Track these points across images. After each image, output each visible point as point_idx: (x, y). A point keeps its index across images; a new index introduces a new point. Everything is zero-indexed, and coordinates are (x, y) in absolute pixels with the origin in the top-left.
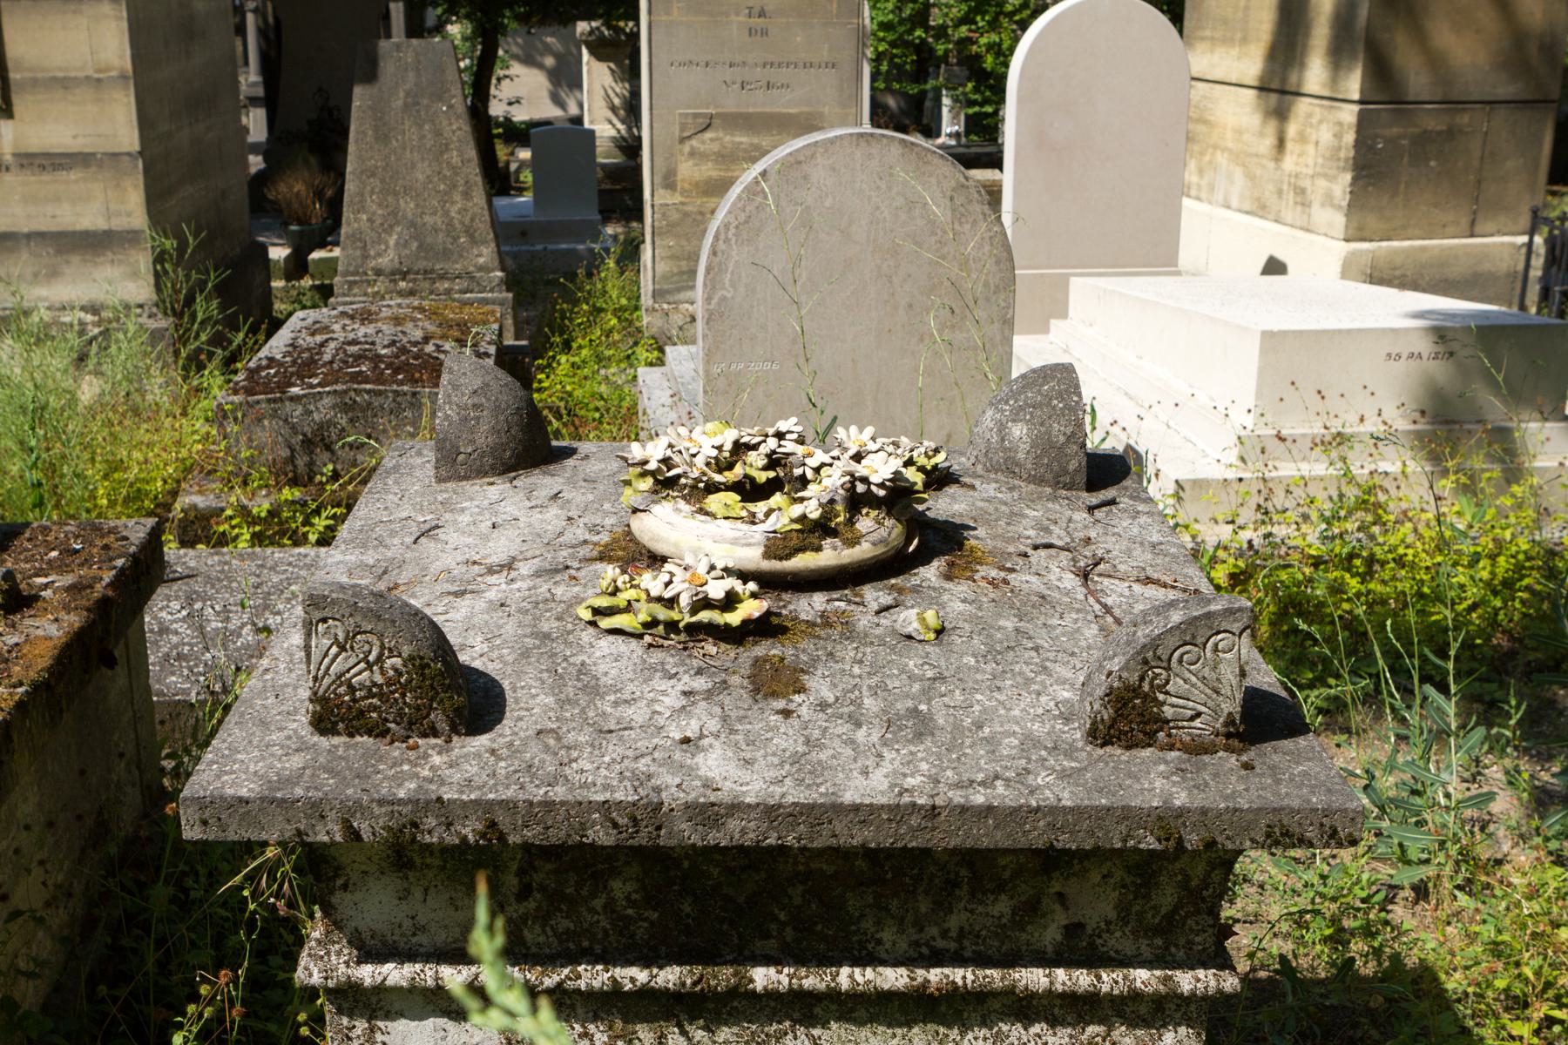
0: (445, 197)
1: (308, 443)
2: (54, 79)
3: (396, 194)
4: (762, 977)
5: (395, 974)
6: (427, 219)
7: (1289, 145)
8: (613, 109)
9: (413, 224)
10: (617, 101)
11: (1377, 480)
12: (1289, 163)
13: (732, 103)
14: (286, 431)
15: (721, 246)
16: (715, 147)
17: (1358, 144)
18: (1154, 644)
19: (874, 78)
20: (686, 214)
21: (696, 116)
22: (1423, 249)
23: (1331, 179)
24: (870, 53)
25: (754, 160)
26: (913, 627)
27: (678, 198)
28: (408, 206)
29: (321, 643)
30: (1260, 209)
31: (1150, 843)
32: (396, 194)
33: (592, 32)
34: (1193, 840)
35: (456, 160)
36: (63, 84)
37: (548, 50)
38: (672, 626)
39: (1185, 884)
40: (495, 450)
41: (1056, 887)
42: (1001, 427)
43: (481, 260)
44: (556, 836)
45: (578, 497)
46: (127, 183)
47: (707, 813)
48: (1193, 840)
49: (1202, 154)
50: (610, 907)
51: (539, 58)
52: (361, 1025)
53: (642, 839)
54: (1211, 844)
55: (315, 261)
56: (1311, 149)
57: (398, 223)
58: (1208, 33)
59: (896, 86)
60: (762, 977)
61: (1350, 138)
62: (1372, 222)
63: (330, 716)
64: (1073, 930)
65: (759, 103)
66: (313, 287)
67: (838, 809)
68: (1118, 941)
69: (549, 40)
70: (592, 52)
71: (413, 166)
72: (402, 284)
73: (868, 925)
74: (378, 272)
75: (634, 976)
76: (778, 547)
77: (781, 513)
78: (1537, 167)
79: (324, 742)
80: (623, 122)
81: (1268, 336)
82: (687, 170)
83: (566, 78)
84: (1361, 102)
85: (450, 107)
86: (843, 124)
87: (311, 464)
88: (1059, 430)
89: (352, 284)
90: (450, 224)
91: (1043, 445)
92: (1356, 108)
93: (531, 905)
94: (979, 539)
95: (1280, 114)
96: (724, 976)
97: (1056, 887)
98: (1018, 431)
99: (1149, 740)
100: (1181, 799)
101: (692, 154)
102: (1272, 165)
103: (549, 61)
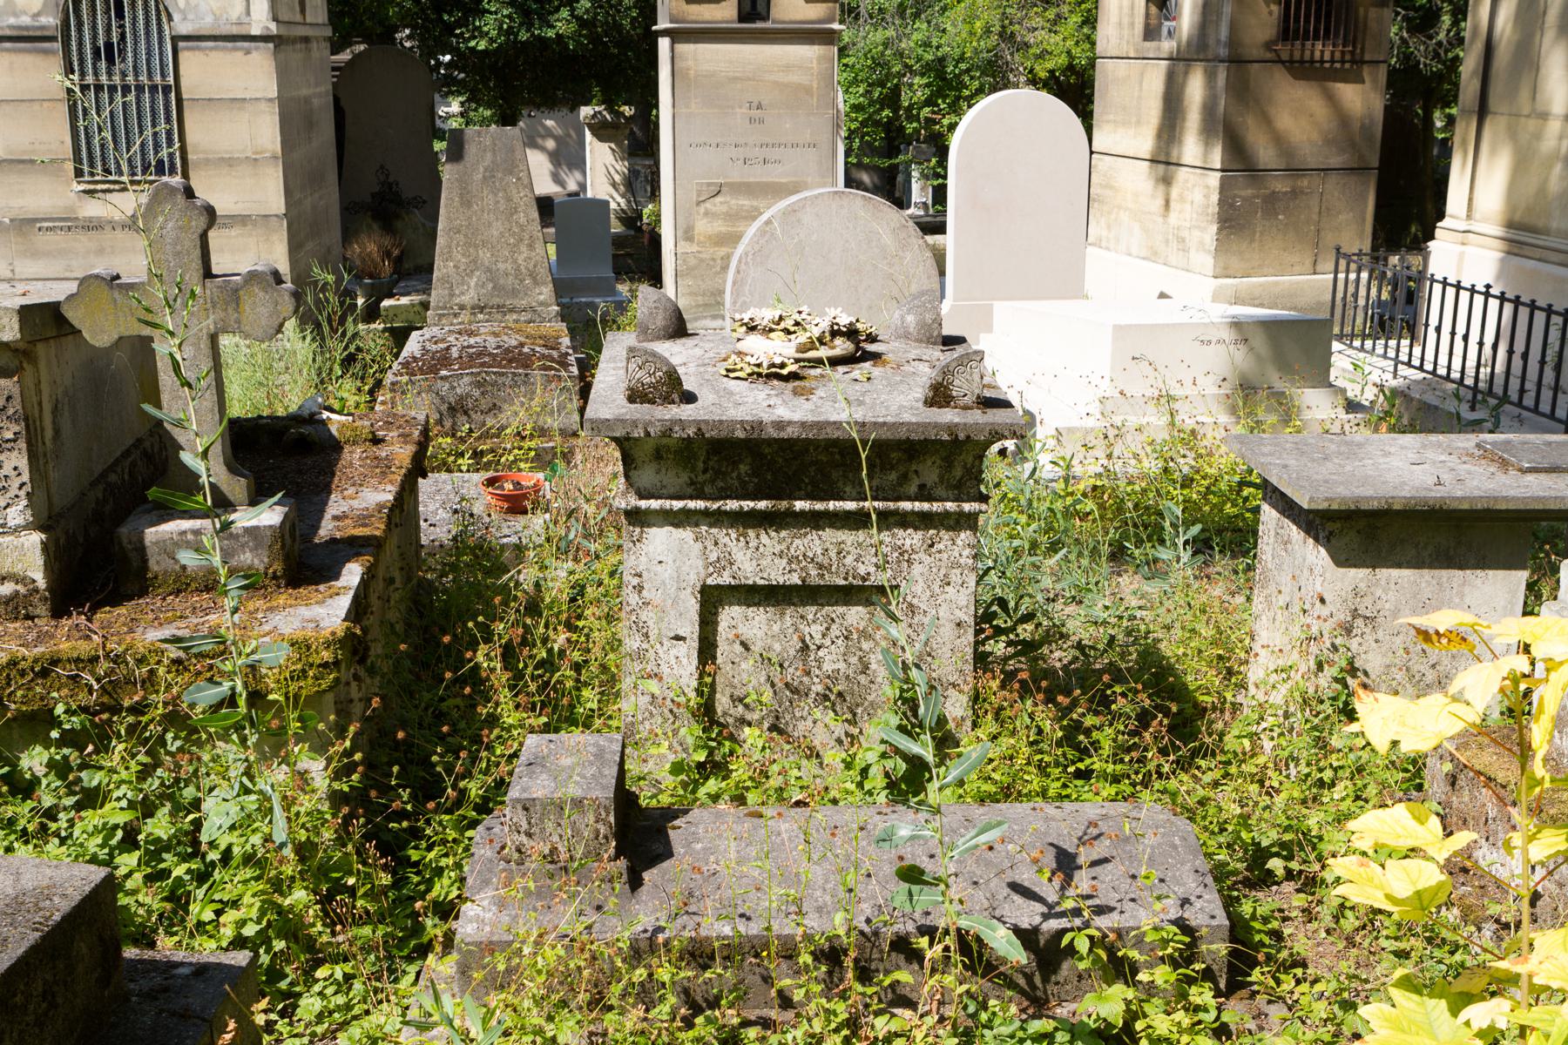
0: (514, 249)
1: (452, 409)
2: (223, 159)
3: (476, 246)
4: (799, 505)
5: (655, 504)
6: (500, 265)
7: (1172, 204)
8: (614, 185)
9: (489, 270)
10: (617, 178)
11: (1472, 638)
12: (1173, 217)
13: (736, 174)
14: (437, 401)
15: (743, 267)
16: (724, 208)
17: (1221, 202)
18: (947, 366)
19: (847, 154)
20: (702, 260)
21: (709, 185)
22: (1276, 283)
23: (1203, 230)
24: (844, 134)
25: (754, 218)
26: (858, 377)
27: (695, 248)
28: (485, 256)
29: (632, 366)
30: (1153, 256)
31: (946, 437)
32: (476, 246)
33: (594, 116)
34: (962, 436)
35: (523, 220)
36: (229, 162)
37: (549, 133)
38: (760, 375)
39: (965, 467)
40: (665, 328)
41: (914, 467)
42: (902, 317)
43: (542, 297)
44: (723, 434)
45: (708, 346)
46: (275, 237)
47: (780, 425)
48: (962, 436)
49: (1109, 213)
50: (739, 477)
51: (540, 141)
52: (638, 530)
53: (755, 436)
54: (968, 437)
55: (386, 309)
56: (1188, 207)
57: (477, 269)
58: (1111, 117)
59: (866, 160)
60: (799, 505)
61: (1215, 197)
62: (1235, 263)
63: (635, 396)
64: (922, 487)
65: (757, 174)
66: (385, 330)
67: (828, 423)
68: (940, 491)
69: (549, 123)
70: (594, 134)
71: (490, 224)
72: (481, 316)
73: (840, 484)
74: (462, 307)
75: (748, 505)
76: (802, 348)
77: (802, 338)
78: (1364, 220)
79: (633, 406)
80: (623, 196)
81: (1118, 328)
82: (703, 227)
83: (569, 158)
84: (1222, 170)
85: (519, 179)
86: (824, 185)
87: (454, 424)
88: (929, 317)
89: (441, 316)
90: (518, 269)
91: (922, 325)
92: (1219, 174)
93: (708, 475)
94: (889, 357)
95: (1167, 181)
96: (784, 505)
97: (914, 467)
98: (910, 318)
99: (947, 405)
100: (957, 420)
101: (706, 214)
102: (1160, 220)
103: (550, 144)
